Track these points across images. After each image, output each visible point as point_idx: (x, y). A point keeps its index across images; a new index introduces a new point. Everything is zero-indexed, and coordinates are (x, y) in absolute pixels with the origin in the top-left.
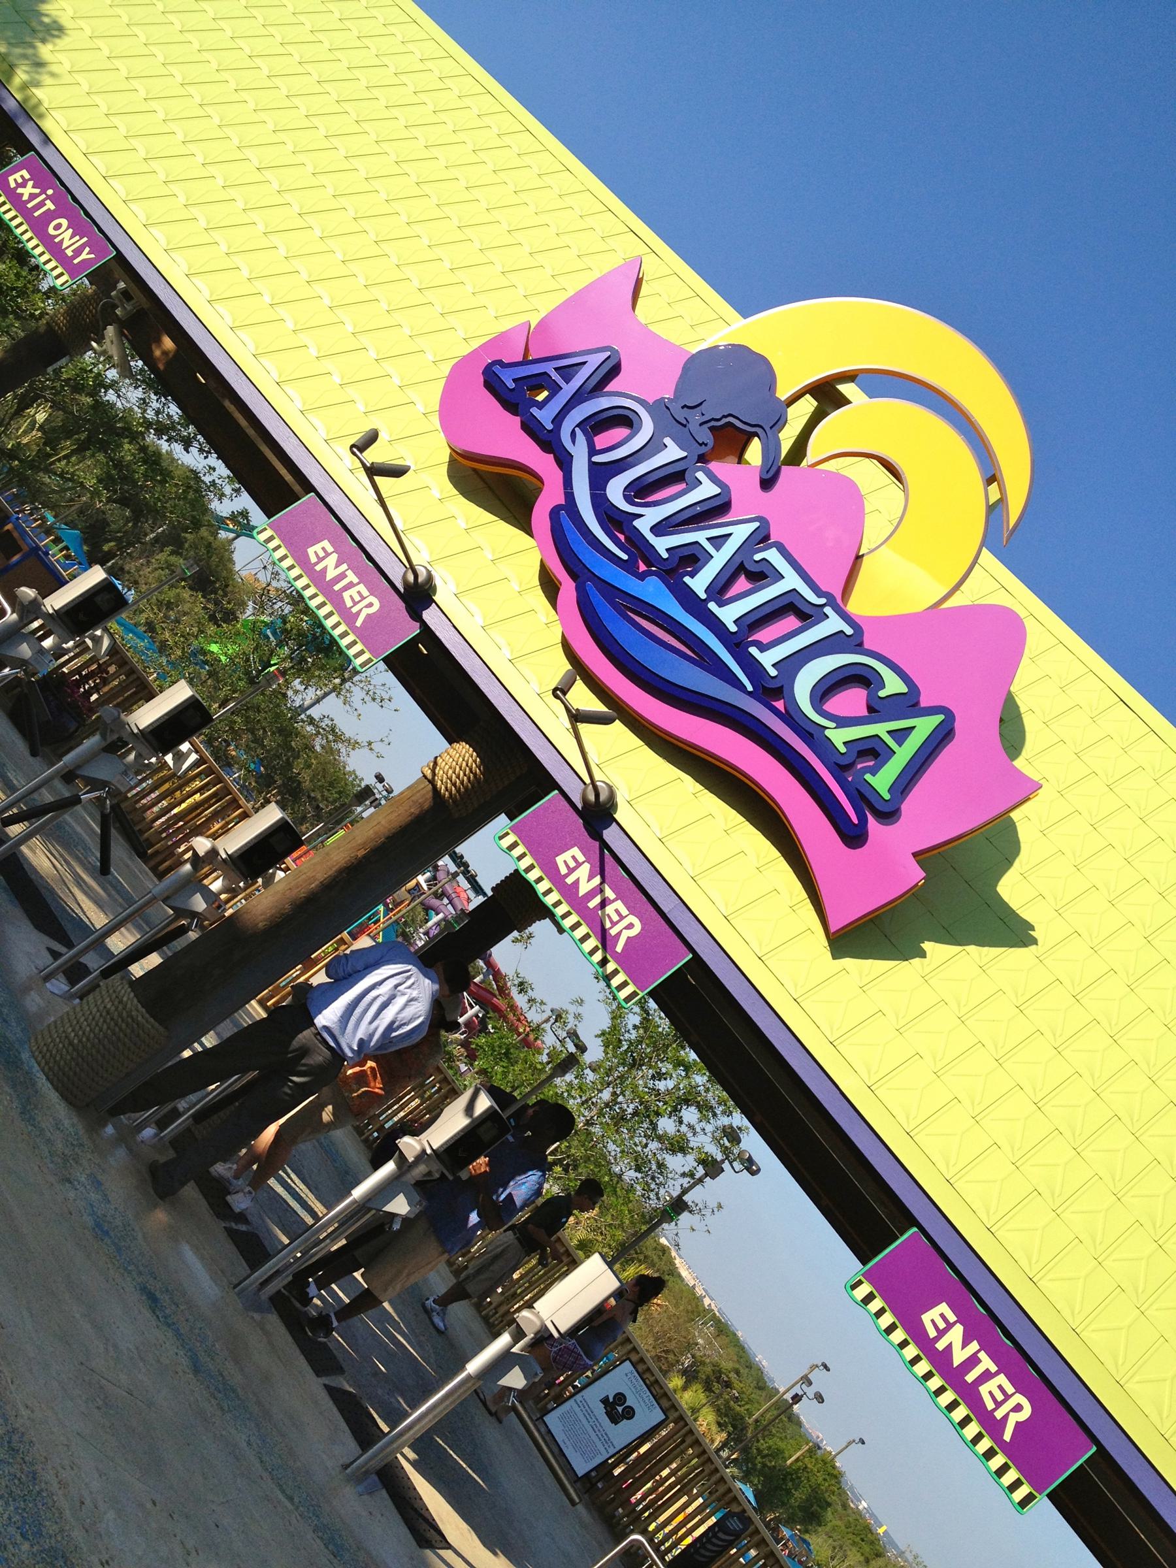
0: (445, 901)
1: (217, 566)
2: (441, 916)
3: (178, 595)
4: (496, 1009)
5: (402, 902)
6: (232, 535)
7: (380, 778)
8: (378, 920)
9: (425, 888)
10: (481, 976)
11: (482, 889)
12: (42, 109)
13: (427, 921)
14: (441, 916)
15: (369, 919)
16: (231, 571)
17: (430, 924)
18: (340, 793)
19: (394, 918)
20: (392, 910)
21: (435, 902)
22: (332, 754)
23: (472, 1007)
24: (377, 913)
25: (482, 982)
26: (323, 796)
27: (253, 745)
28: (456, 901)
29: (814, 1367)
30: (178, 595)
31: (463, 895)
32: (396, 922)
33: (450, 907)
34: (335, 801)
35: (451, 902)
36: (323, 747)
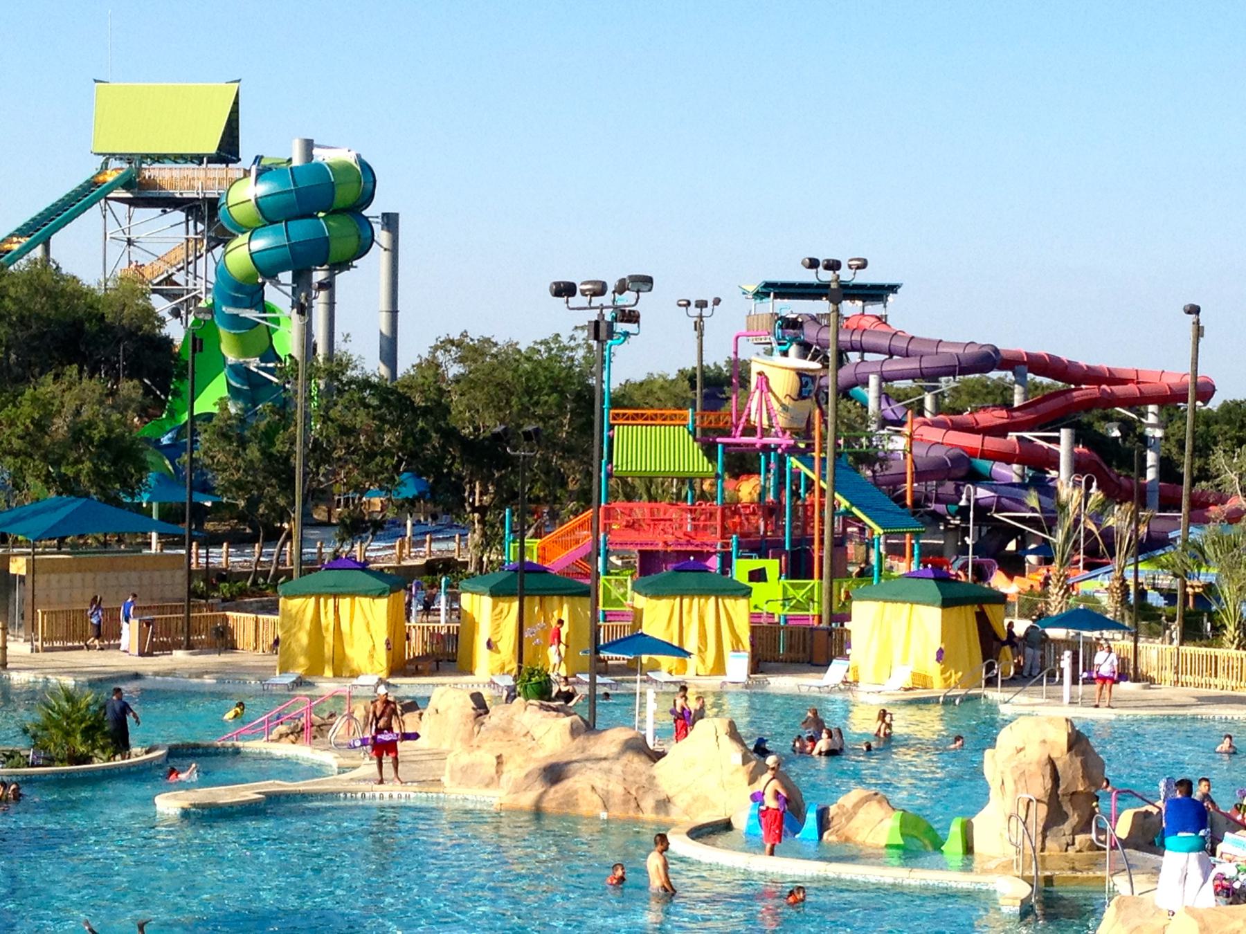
0: (854, 357)
1: (57, 308)
2: (873, 380)
3: (35, 400)
4: (1089, 405)
5: (809, 423)
6: (38, 252)
7: (813, 264)
8: (810, 484)
9: (816, 365)
10: (1018, 389)
11: (881, 287)
12: (417, 361)
13: (864, 406)
14: (873, 380)
15: (795, 494)
16: (81, 293)
17: (872, 405)
18: (554, 389)
19: (829, 456)
20: (810, 447)
21: (846, 373)
22: (483, 354)
23: (1057, 440)
24: (796, 475)
25: (1026, 394)
26: (541, 418)
27: (372, 467)
28: (868, 340)
29: (436, 348)
30: (35, 400)
31: (867, 323)
32: (838, 455)
33: (868, 356)
34: (561, 407)
35: (862, 349)
36: (461, 360)
